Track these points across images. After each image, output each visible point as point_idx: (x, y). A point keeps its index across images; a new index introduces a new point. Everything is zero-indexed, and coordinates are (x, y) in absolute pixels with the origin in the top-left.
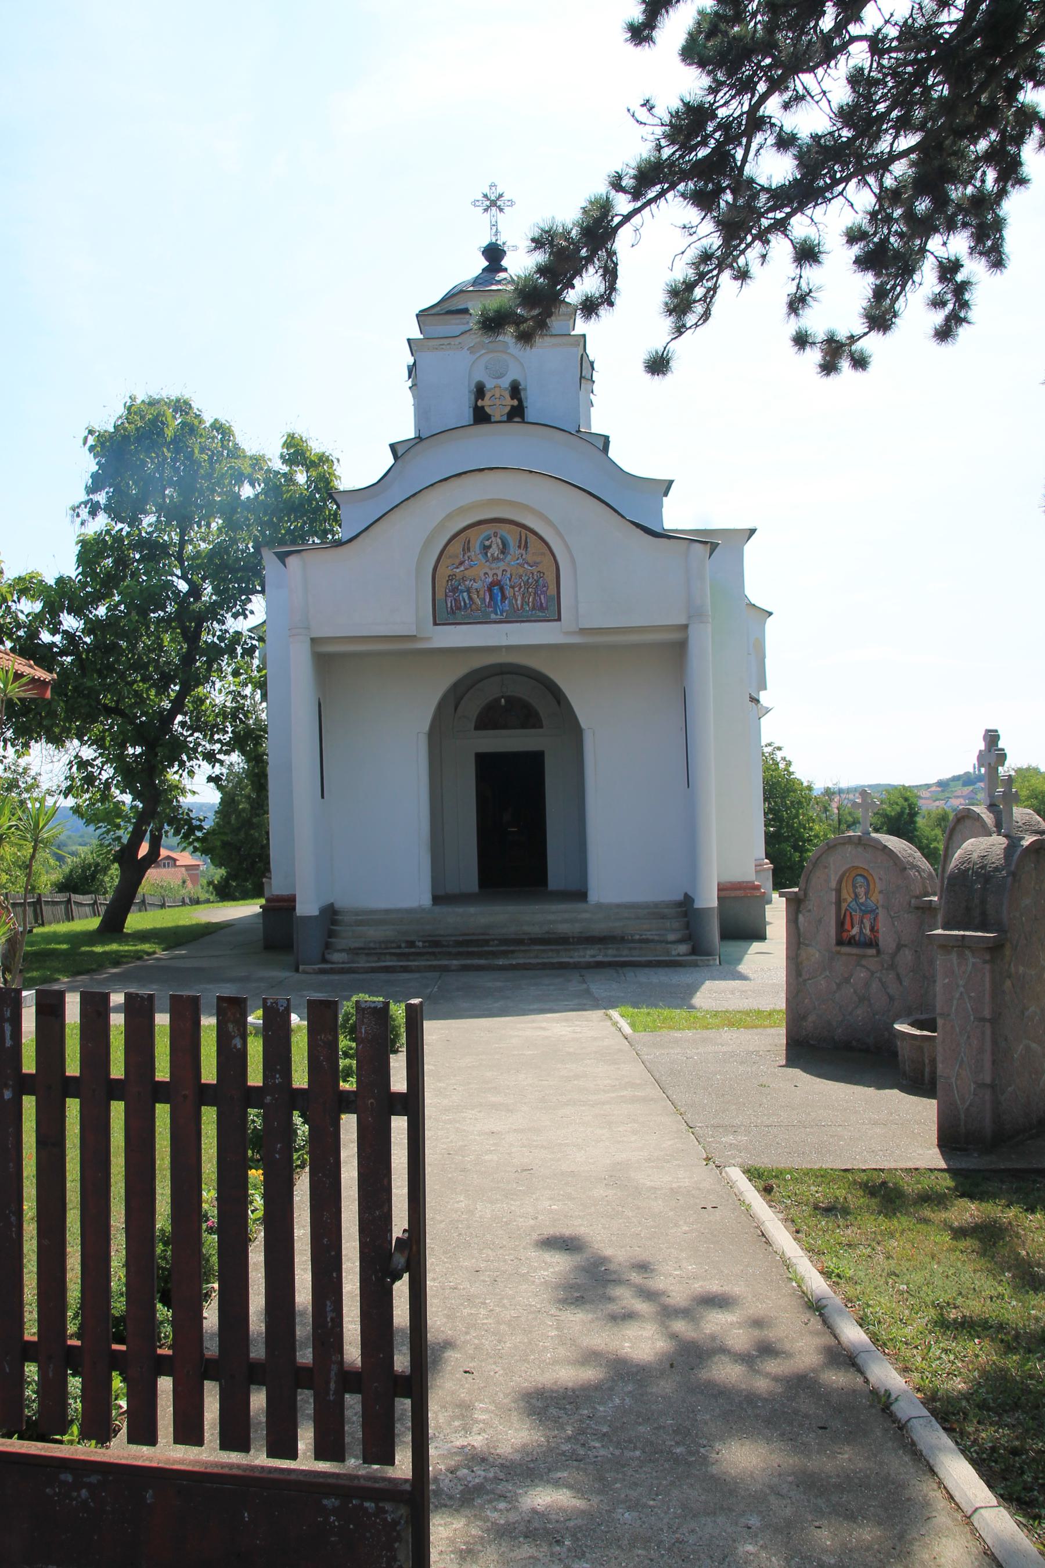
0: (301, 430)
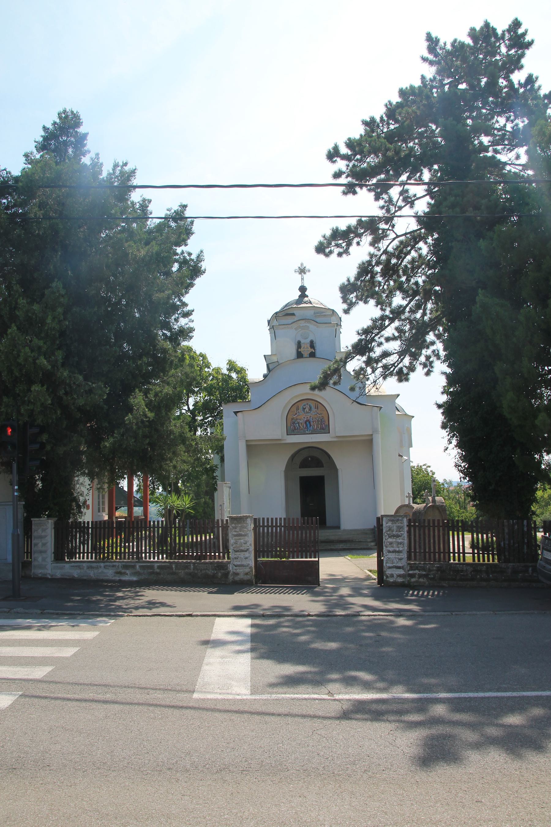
0: (233, 359)
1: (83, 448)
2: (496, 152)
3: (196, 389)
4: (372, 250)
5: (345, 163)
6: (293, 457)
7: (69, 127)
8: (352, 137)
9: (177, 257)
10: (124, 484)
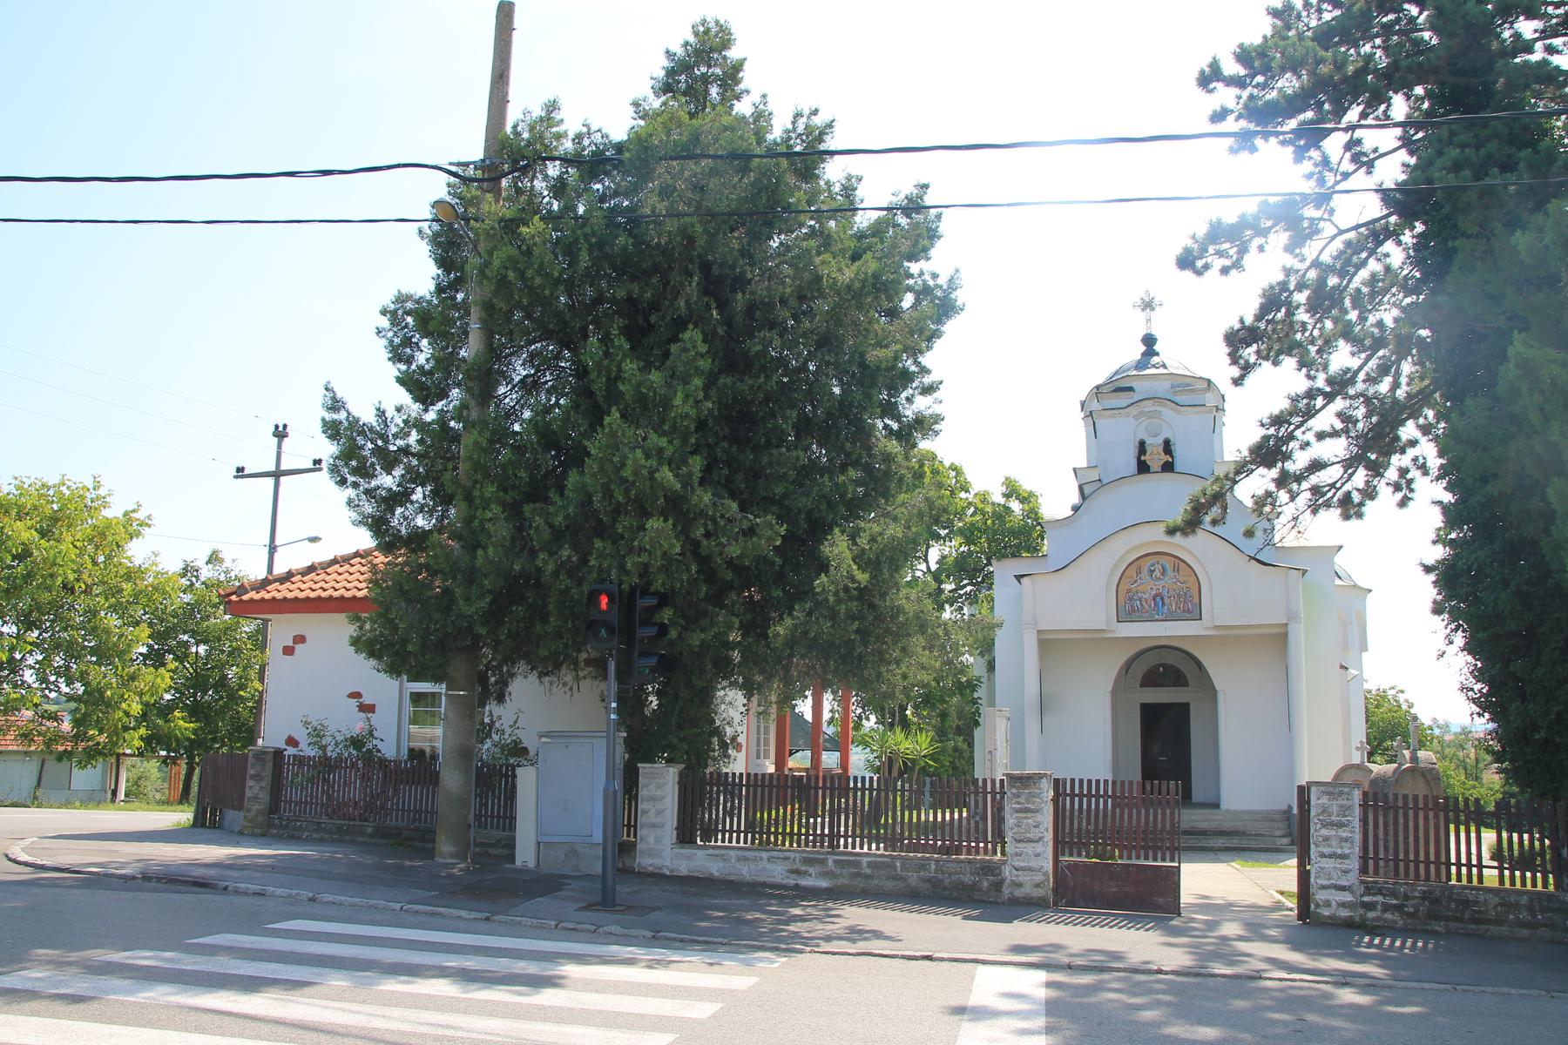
1: (734, 636)
2: (1550, 50)
3: (943, 532)
4: (1290, 261)
5: (1234, 91)
6: (1128, 666)
7: (712, 50)
8: (1247, 42)
9: (911, 282)
10: (805, 708)
